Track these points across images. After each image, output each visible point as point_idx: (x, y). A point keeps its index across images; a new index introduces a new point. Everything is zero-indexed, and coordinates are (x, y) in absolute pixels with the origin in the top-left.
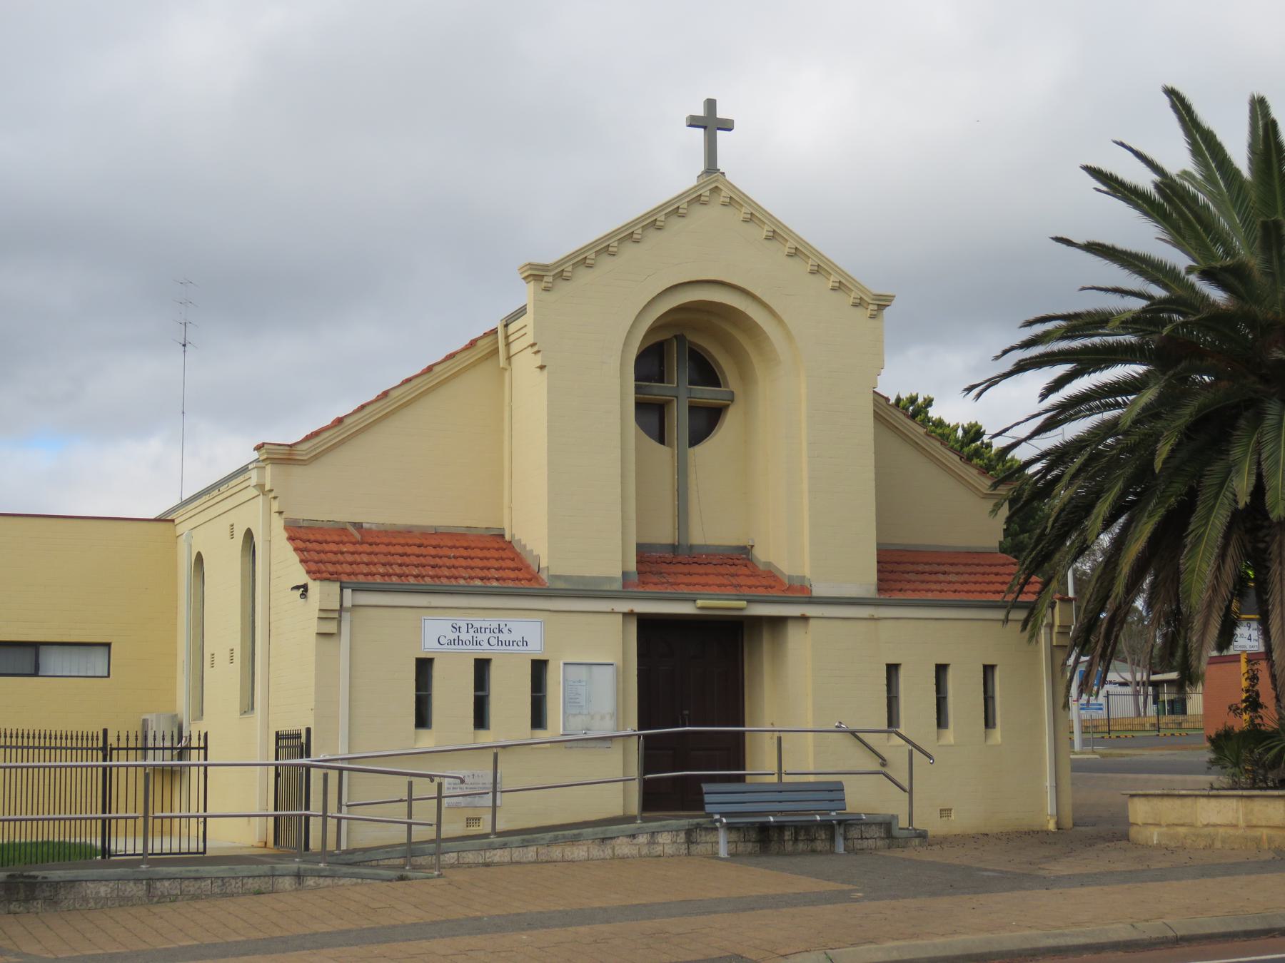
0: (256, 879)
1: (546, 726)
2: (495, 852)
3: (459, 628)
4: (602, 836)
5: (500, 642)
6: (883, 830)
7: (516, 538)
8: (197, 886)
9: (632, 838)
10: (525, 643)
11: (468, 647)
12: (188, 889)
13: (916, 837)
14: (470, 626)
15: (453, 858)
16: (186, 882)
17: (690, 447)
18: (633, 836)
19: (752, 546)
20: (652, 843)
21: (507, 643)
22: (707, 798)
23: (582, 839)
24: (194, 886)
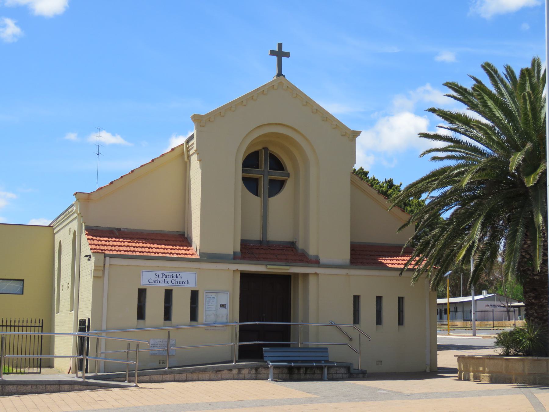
0: (52, 386)
1: (171, 320)
2: (167, 376)
3: (158, 275)
4: (216, 370)
5: (177, 282)
6: (346, 370)
7: (189, 236)
8: (24, 388)
9: (230, 371)
11: (162, 284)
12: (20, 390)
13: (361, 373)
14: (163, 275)
15: (148, 378)
16: (19, 387)
17: (269, 197)
18: (231, 370)
19: (296, 242)
21: (180, 283)
22: (265, 354)
23: (207, 371)
24: (23, 388)
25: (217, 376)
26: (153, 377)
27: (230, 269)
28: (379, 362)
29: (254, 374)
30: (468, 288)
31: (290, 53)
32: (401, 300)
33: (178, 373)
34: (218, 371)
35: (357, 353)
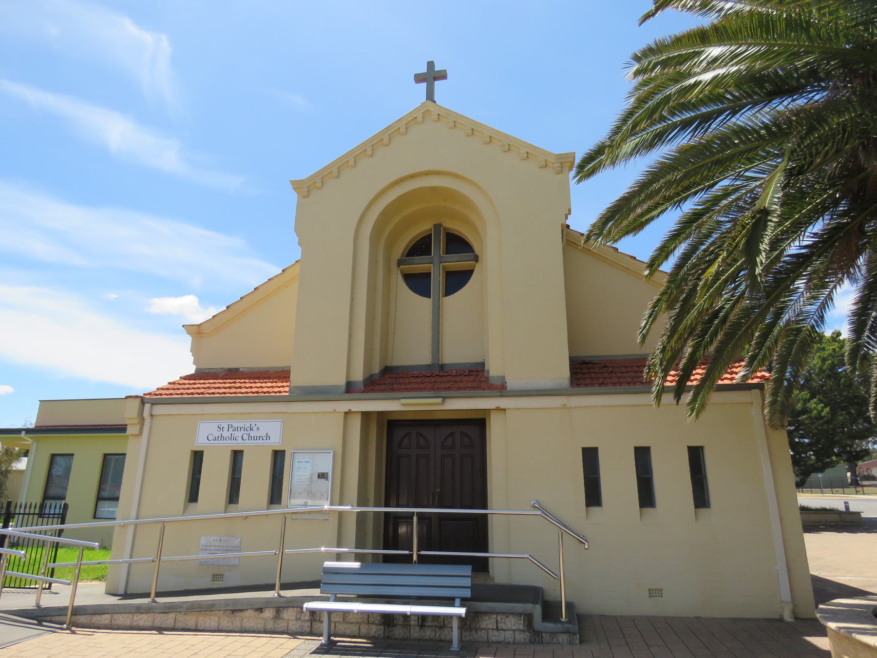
2: (141, 616)
3: (223, 428)
4: (233, 609)
6: (522, 622)
10: (268, 438)
13: (563, 633)
14: (230, 426)
18: (260, 610)
20: (277, 617)
25: (232, 622)
26: (116, 616)
27: (337, 410)
28: (655, 593)
29: (307, 621)
30: (874, 418)
31: (433, 61)
32: (696, 455)
33: (160, 612)
34: (235, 609)
35: (555, 578)
